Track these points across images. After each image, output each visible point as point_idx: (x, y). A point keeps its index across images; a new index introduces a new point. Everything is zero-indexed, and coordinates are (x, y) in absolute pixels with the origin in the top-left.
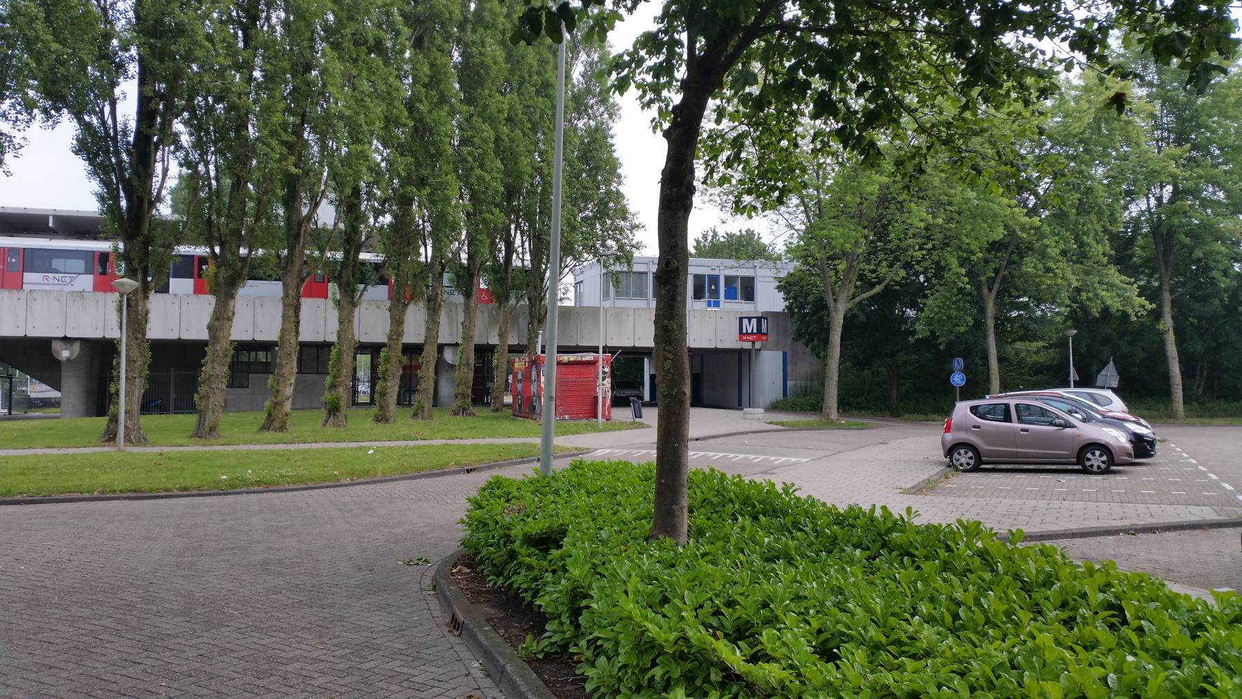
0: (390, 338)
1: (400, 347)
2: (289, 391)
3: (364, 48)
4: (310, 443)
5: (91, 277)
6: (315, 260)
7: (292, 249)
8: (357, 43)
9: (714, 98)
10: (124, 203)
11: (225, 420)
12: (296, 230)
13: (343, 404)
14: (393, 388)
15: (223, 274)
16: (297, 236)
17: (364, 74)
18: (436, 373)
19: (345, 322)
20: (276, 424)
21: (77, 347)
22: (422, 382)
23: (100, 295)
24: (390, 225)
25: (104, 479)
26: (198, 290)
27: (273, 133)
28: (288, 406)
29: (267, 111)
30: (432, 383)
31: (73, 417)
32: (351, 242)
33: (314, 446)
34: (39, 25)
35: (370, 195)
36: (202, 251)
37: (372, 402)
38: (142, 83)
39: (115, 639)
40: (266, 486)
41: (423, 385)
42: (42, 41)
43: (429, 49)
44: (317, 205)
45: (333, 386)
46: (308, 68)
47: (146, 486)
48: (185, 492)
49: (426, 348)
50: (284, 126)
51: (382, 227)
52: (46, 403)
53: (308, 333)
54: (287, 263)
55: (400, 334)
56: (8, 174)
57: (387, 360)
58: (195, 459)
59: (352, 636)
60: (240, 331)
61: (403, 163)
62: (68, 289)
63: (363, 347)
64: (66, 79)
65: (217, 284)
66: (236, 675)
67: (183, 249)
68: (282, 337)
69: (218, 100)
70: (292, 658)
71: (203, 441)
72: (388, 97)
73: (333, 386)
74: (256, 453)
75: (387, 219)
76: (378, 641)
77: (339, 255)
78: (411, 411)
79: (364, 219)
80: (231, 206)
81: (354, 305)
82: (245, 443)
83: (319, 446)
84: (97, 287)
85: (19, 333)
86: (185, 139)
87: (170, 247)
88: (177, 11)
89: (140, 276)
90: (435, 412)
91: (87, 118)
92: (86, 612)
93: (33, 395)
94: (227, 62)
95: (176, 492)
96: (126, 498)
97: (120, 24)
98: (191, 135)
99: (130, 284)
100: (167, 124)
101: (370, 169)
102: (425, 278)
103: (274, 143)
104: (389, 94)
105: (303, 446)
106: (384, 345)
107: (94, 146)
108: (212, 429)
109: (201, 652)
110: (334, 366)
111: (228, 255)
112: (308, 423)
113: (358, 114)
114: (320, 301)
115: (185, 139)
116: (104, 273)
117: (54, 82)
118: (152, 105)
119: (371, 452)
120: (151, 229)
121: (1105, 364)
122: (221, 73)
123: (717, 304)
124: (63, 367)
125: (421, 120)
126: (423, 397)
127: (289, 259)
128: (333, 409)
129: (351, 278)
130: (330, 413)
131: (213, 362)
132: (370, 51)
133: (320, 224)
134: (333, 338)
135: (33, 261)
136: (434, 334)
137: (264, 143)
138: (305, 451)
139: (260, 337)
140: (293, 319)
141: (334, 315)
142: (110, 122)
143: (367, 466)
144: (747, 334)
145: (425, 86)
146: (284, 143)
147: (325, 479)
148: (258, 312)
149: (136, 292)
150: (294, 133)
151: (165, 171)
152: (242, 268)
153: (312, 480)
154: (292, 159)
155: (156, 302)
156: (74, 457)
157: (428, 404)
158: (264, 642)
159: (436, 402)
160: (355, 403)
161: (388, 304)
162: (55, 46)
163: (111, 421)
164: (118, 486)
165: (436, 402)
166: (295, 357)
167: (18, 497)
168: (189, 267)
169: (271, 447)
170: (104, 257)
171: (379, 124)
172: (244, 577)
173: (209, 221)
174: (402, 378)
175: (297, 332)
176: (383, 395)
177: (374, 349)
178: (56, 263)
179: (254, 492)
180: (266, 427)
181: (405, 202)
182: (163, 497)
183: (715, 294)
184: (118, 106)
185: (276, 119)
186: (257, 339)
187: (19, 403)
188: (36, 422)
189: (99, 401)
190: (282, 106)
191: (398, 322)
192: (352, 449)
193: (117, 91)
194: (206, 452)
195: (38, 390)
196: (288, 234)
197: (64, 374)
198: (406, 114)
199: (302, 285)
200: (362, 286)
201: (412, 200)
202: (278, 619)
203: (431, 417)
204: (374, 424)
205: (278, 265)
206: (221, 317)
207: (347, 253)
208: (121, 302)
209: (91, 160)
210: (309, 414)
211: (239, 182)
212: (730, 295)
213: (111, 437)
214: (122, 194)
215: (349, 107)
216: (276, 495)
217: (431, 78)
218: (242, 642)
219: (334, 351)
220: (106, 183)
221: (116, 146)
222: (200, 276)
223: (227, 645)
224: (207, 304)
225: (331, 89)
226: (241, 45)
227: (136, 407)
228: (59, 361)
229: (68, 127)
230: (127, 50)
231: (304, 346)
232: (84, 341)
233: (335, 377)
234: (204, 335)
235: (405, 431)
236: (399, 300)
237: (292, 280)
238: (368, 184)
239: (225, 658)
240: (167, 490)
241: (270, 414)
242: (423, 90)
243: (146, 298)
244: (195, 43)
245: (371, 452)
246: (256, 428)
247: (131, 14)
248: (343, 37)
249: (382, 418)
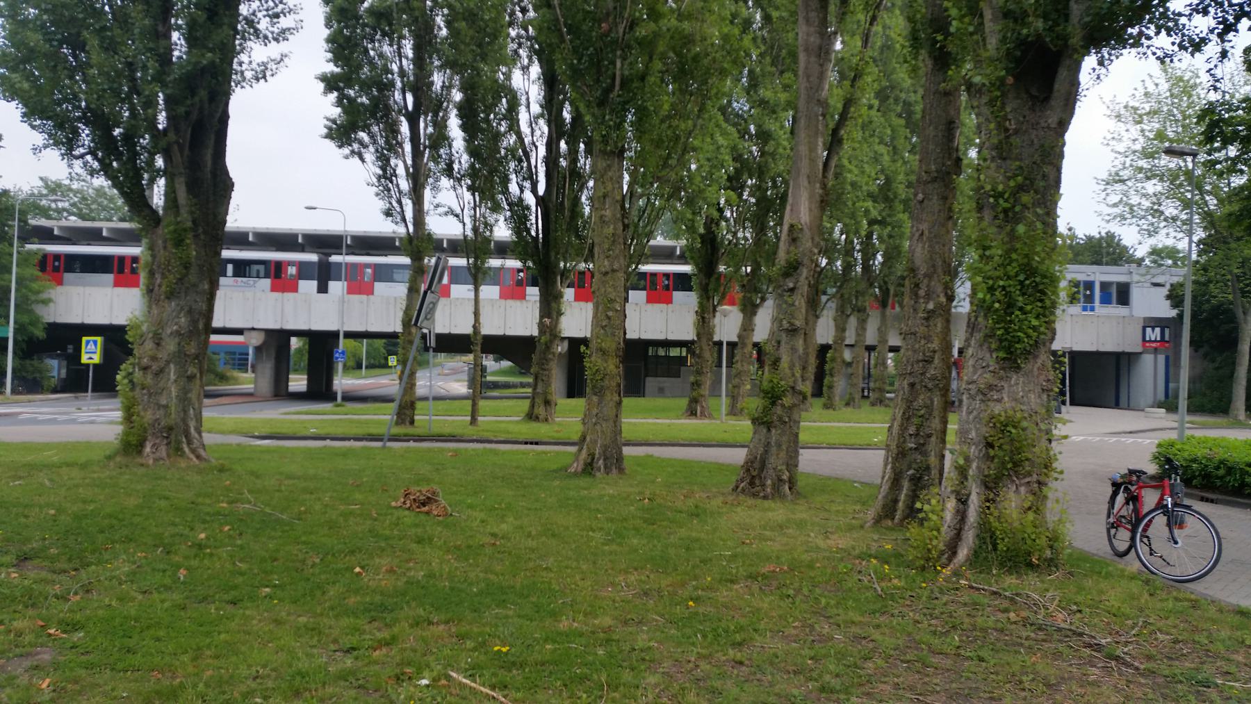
21: (566, 344)
95: (1171, 385)
121: (165, 208)
123: (1092, 309)
144: (1150, 341)
183: (1089, 299)
203: (860, 407)
212: (1106, 300)
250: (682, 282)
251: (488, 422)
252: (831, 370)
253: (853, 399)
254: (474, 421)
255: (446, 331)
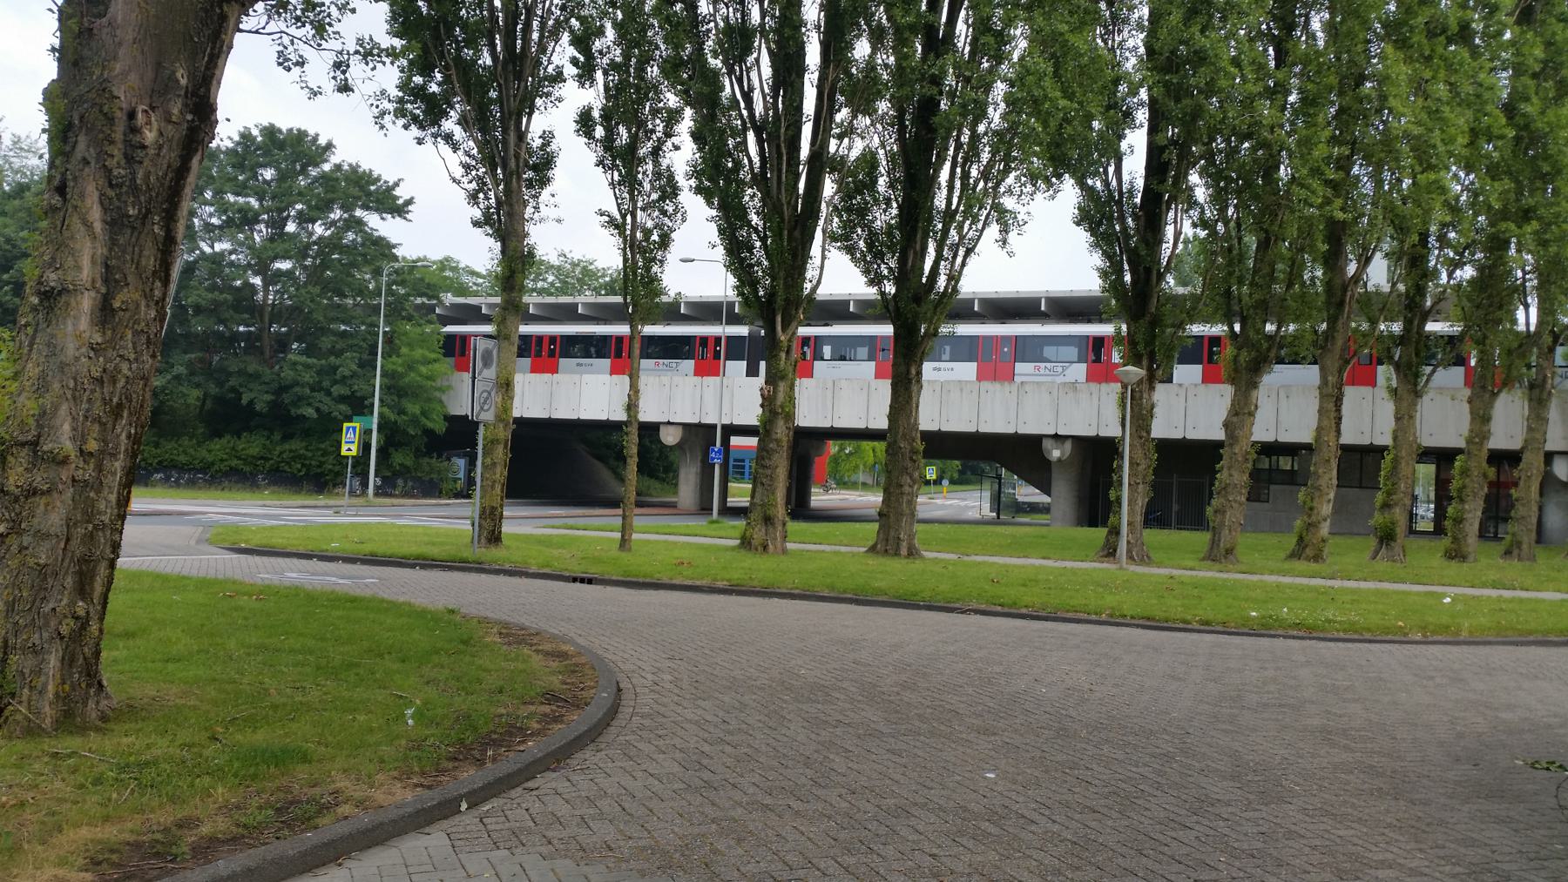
0: (1469, 441)
1: (1485, 455)
2: (1326, 509)
3: (1442, 39)
4: (1353, 582)
5: (873, 363)
6: (1364, 335)
7: (1333, 321)
8: (1431, 34)
9: (1318, 12)
10: (1128, 278)
11: (1244, 541)
12: (1339, 295)
13: (1401, 529)
14: (1474, 511)
15: (1244, 356)
16: (1341, 304)
17: (1442, 74)
18: (1541, 495)
19: (1404, 418)
20: (1308, 551)
21: (1068, 445)
22: (1518, 506)
23: (1094, 386)
24: (1472, 281)
25: (1110, 600)
26: (1208, 378)
27: (1316, 172)
28: (1325, 529)
29: (1306, 143)
30: (1535, 508)
31: (1062, 527)
32: (1413, 308)
33: (1363, 585)
34: (1048, 83)
35: (1443, 240)
36: (1218, 329)
37: (1439, 530)
38: (1152, 131)
39: (1158, 793)
40: (1308, 631)
41: (1519, 511)
42: (1051, 100)
43: (1544, 21)
44: (1368, 260)
45: (1386, 506)
46: (1361, 79)
47: (1158, 614)
48: (1206, 627)
49: (1526, 457)
50: (1328, 159)
51: (1459, 285)
52: (1034, 508)
53: (1353, 432)
54: (1326, 339)
55: (1485, 436)
56: (1011, 254)
57: (1465, 472)
58: (1214, 587)
59: (1463, 850)
60: (1263, 431)
61: (1496, 193)
62: (1059, 380)
63: (1427, 454)
64: (1072, 139)
65: (1236, 370)
66: (1310, 868)
67: (1196, 329)
68: (1318, 438)
69: (1244, 137)
70: (1382, 862)
71: (1218, 566)
72: (1477, 102)
73: (1386, 506)
74: (1290, 586)
75: (1468, 272)
76: (1505, 867)
77: (1397, 328)
78: (1500, 548)
79: (1435, 273)
80: (1256, 271)
81: (1417, 394)
82: (1272, 573)
83: (1371, 585)
84: (1091, 377)
85: (1009, 429)
86: (1201, 194)
87: (1181, 326)
88: (1198, 35)
89: (1145, 362)
90: (1540, 552)
91: (1090, 182)
92: (1120, 755)
93: (1020, 499)
94: (1252, 88)
95: (1196, 626)
96: (1138, 626)
97: (1131, 64)
98: (1207, 186)
99: (1135, 372)
100: (1182, 176)
101: (1446, 204)
102: (1523, 356)
103: (1315, 184)
104: (1478, 96)
105: (1351, 584)
106: (1459, 451)
107: (1097, 216)
108: (1229, 551)
109: (1264, 830)
110: (1387, 478)
111: (1251, 334)
112: (1352, 552)
113: (1431, 130)
114: (1365, 390)
115: (1201, 194)
116: (1098, 360)
117: (1058, 145)
118: (1165, 156)
119: (1448, 600)
120: (1160, 305)
122: (1248, 103)
124: (1055, 470)
125: (1526, 127)
126: (1521, 527)
127: (1329, 335)
128: (1386, 537)
129: (1414, 358)
130: (1381, 542)
131: (1229, 468)
132: (1450, 41)
133: (1370, 288)
134: (1385, 439)
135: (1027, 349)
136: (1538, 436)
137: (1302, 186)
138: (1354, 591)
139: (1285, 438)
140: (1333, 415)
141: (1387, 409)
142: (1114, 183)
143: (1445, 620)
145: (1535, 76)
146: (1328, 183)
147: (1387, 630)
148: (1287, 406)
149: (1140, 382)
150: (1338, 168)
151: (1177, 234)
152: (1269, 350)
153: (1369, 630)
154: (1339, 202)
155: (1161, 393)
156: (1074, 571)
157: (1528, 538)
158: (1341, 833)
159: (1540, 536)
160: (1412, 532)
161: (1467, 392)
162: (1063, 103)
163: (1110, 533)
164: (1128, 609)
165: (1540, 536)
166: (1334, 464)
167: (1024, 611)
168: (1202, 351)
169: (1305, 581)
170: (1098, 342)
171: (1462, 140)
172: (1301, 745)
173: (1228, 293)
174: (1487, 499)
175: (1338, 432)
176: (1459, 521)
177: (1443, 457)
178: (1049, 351)
179: (1294, 637)
180: (1296, 555)
181: (1497, 245)
182: (1180, 630)
184: (1124, 163)
185: (1320, 151)
186: (1189, 437)
187: (1008, 507)
188: (1025, 528)
189: (1095, 507)
190: (1327, 133)
191: (1481, 418)
192: (1418, 594)
193: (1124, 145)
194: (1225, 580)
195: (1027, 493)
196: (1328, 303)
197: (1055, 475)
198: (1504, 121)
199: (1345, 366)
200: (1428, 369)
201: (1508, 242)
202: (1353, 806)
203: (1533, 559)
204: (1446, 563)
205: (1315, 344)
206: (1241, 412)
207: (1408, 323)
208: (1123, 394)
209: (1093, 231)
210: (1350, 541)
211: (1267, 240)
213: (1110, 552)
214: (1126, 267)
215: (1419, 123)
216: (1322, 644)
217: (1545, 62)
218: (1311, 827)
219: (1389, 458)
220: (1107, 255)
221: (1121, 211)
222: (1210, 361)
223: (1293, 828)
224: (1220, 398)
225: (1392, 102)
226: (1272, 64)
227: (1139, 519)
228: (1049, 462)
229: (1069, 192)
230: (1136, 94)
231: (1347, 450)
232: (1076, 440)
233: (1389, 494)
234: (1218, 434)
235: (1493, 575)
236: (1484, 387)
237: (1333, 362)
238: (1444, 225)
239: (1291, 843)
240: (1185, 621)
241: (1301, 539)
242: (1531, 83)
243: (1152, 388)
244: (1218, 70)
245: (1448, 600)
246: (1282, 555)
247: (1142, 50)
248: (1412, 29)
249: (1456, 554)
250: (736, 348)
251: (527, 539)
252: (1460, 490)
253: (1519, 544)
254: (624, 543)
255: (1177, 434)
